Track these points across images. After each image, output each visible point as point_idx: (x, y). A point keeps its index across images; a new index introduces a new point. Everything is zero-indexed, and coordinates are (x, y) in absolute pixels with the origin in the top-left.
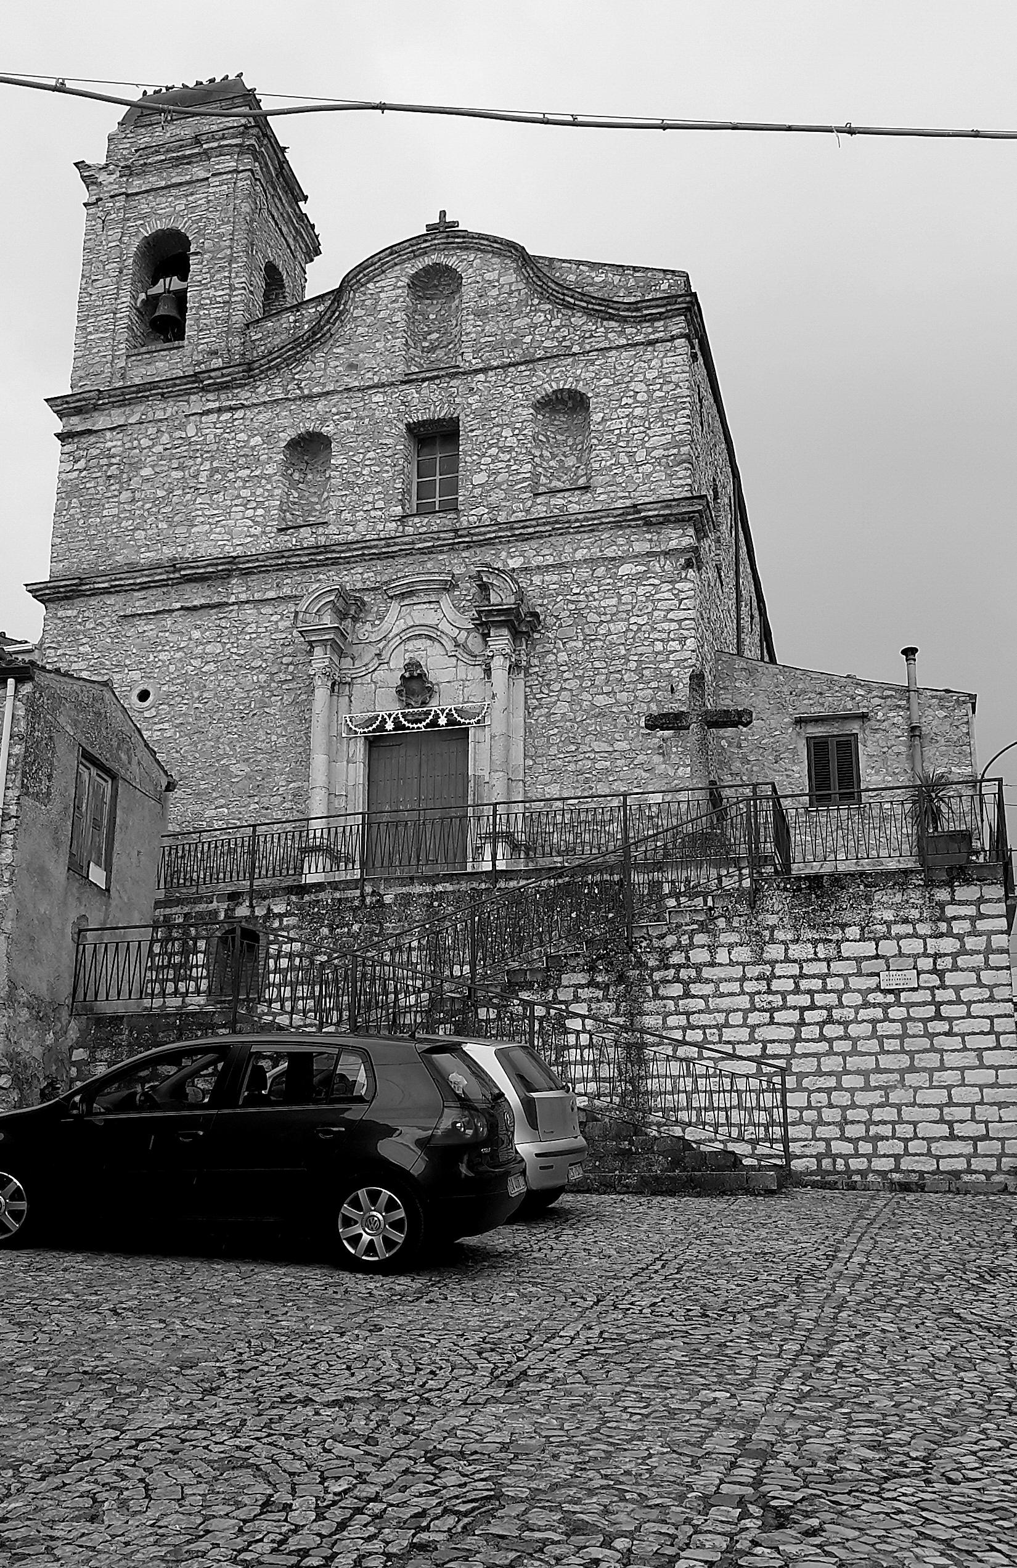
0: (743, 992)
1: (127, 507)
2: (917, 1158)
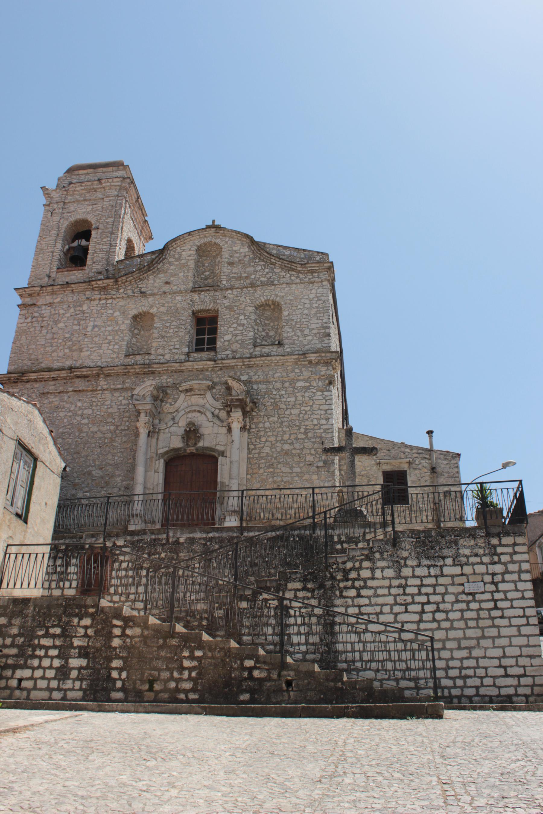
0: (390, 594)
1: (49, 341)
2: (488, 688)
